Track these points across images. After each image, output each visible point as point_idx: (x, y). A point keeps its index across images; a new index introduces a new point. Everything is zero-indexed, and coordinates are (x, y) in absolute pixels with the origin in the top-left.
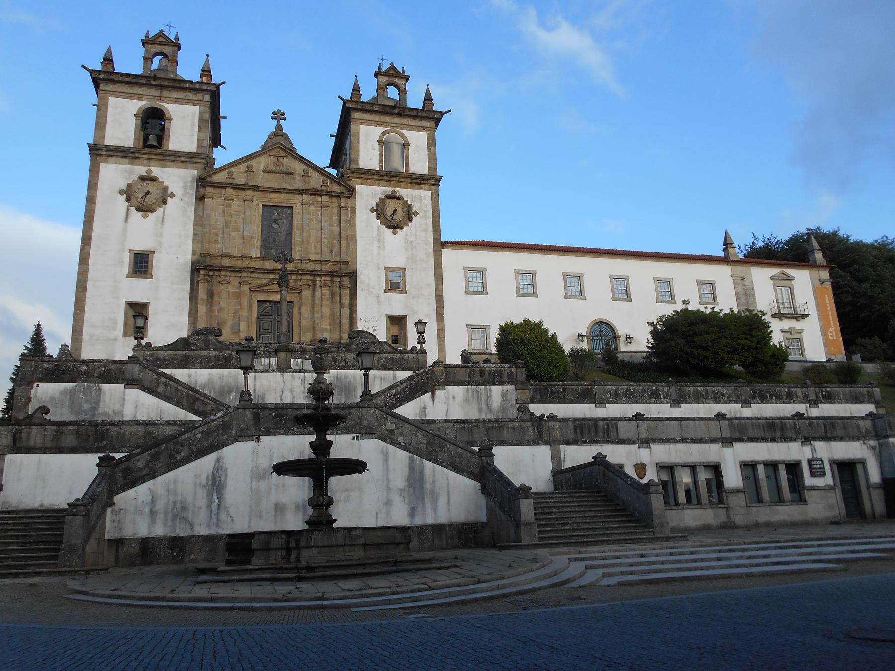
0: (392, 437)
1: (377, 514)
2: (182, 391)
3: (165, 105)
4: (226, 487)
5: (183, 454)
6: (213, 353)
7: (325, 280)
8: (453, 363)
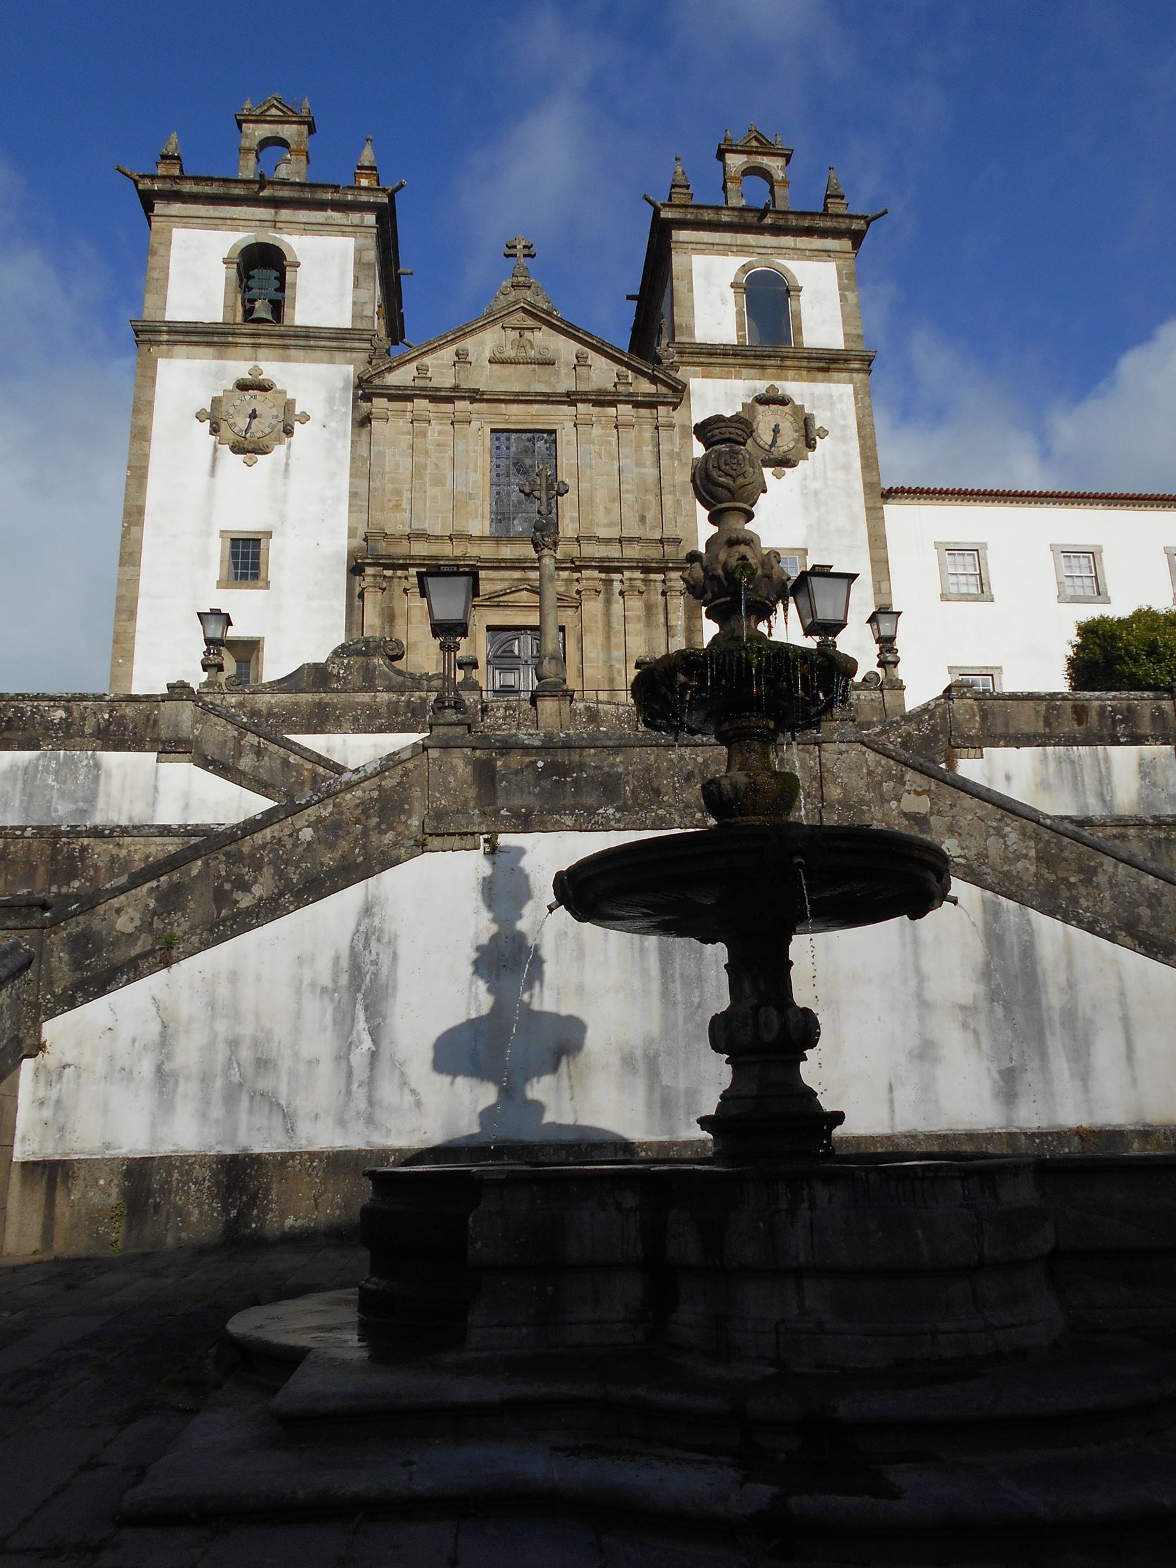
1: (891, 1089)
2: (299, 769)
3: (286, 238)
4: (394, 996)
5: (258, 891)
6: (384, 697)
7: (631, 579)
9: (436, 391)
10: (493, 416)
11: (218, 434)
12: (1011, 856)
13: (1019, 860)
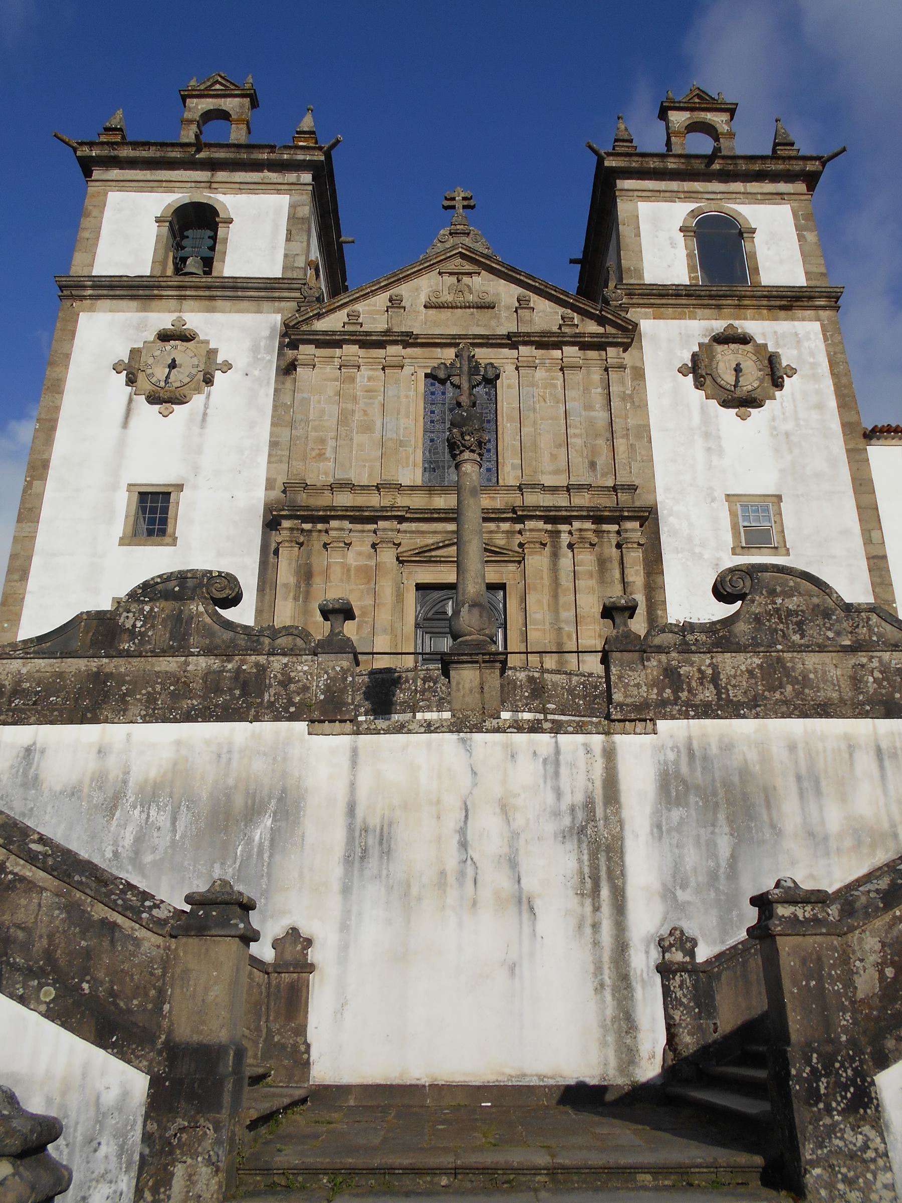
6: (200, 664)
7: (581, 530)
9: (366, 335)
10: (427, 360)
11: (134, 384)
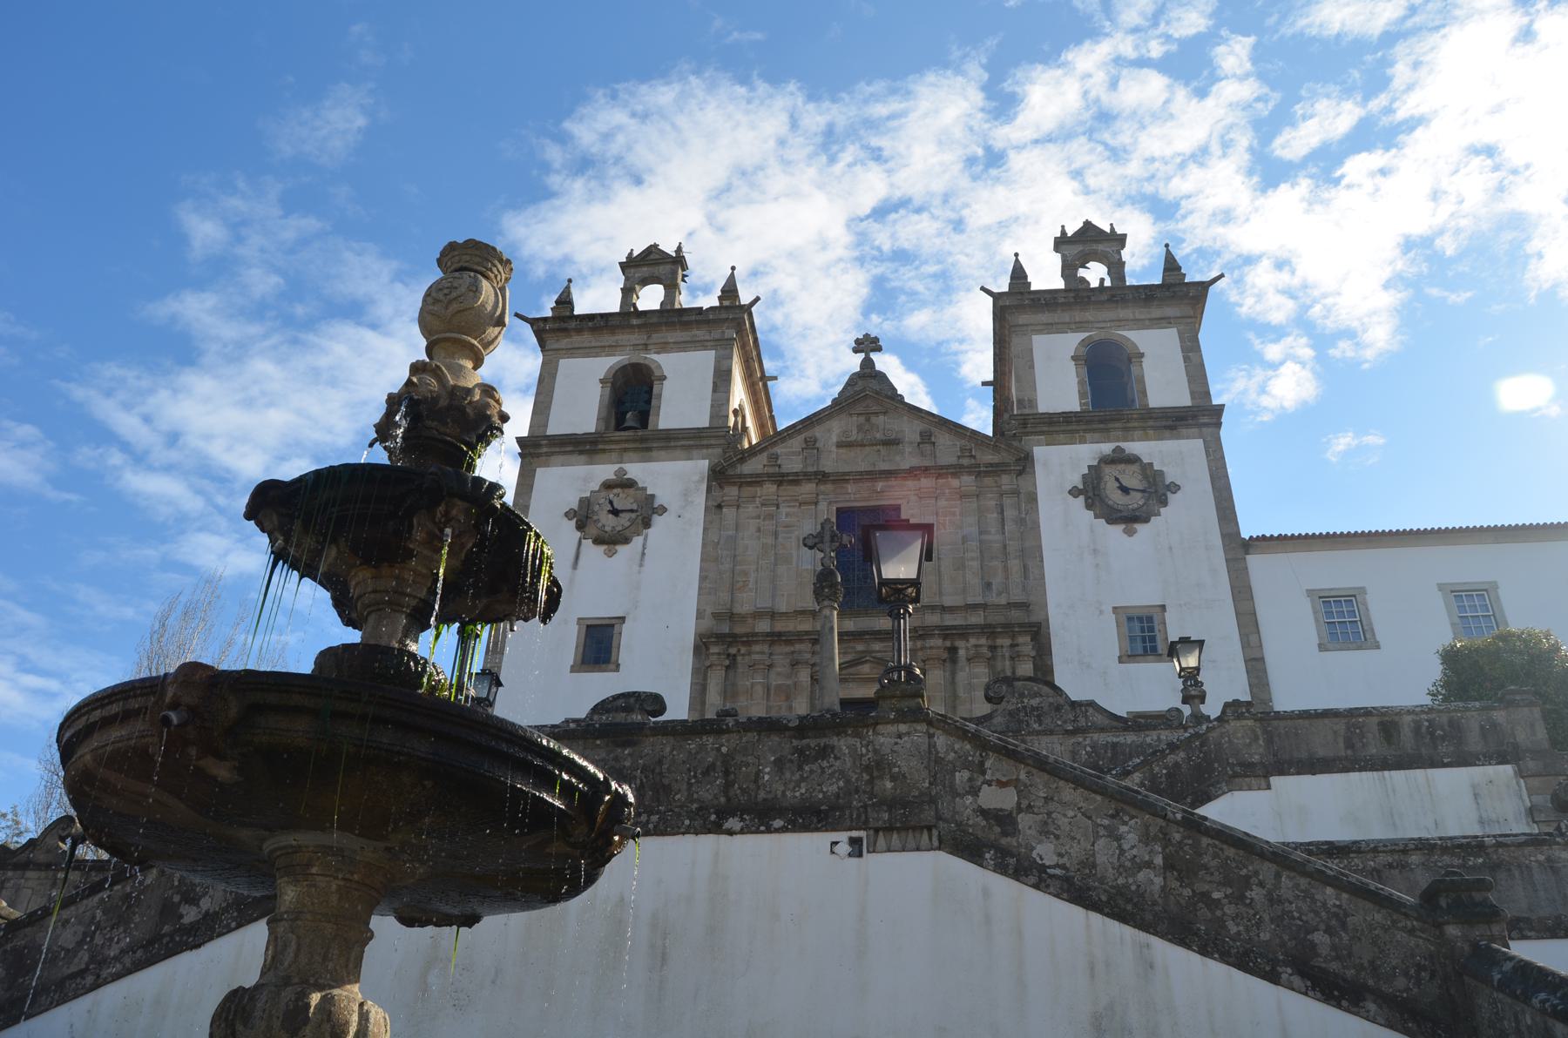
0: (1004, 841)
7: (976, 646)
8: (1289, 709)
12: (1128, 864)
13: (1140, 869)
